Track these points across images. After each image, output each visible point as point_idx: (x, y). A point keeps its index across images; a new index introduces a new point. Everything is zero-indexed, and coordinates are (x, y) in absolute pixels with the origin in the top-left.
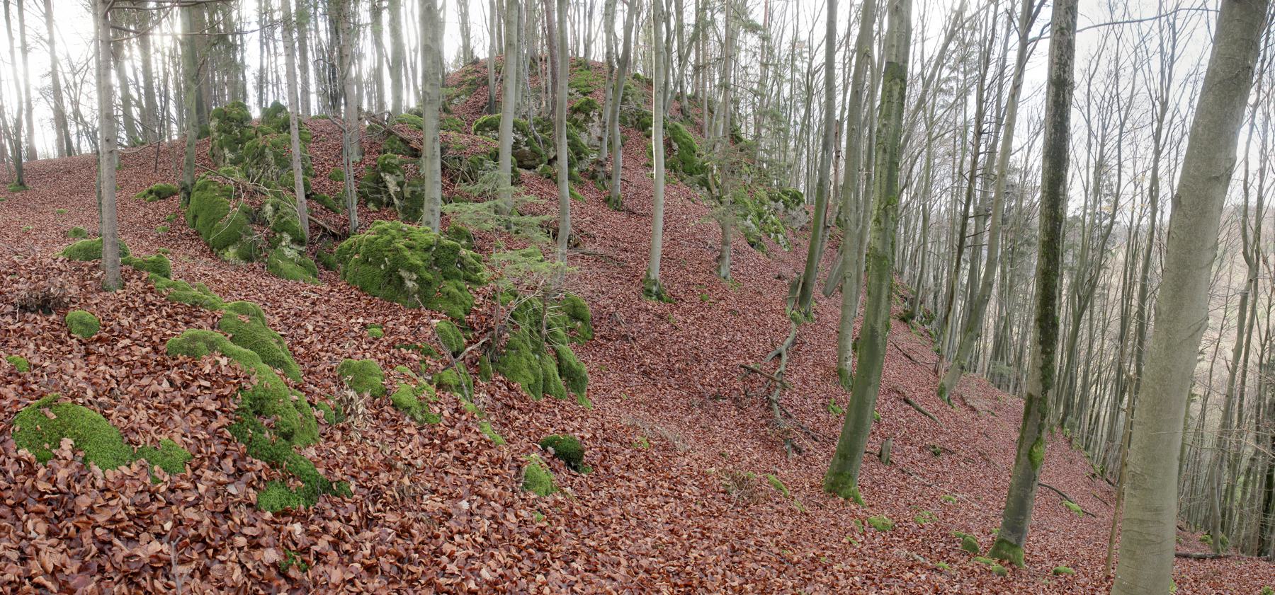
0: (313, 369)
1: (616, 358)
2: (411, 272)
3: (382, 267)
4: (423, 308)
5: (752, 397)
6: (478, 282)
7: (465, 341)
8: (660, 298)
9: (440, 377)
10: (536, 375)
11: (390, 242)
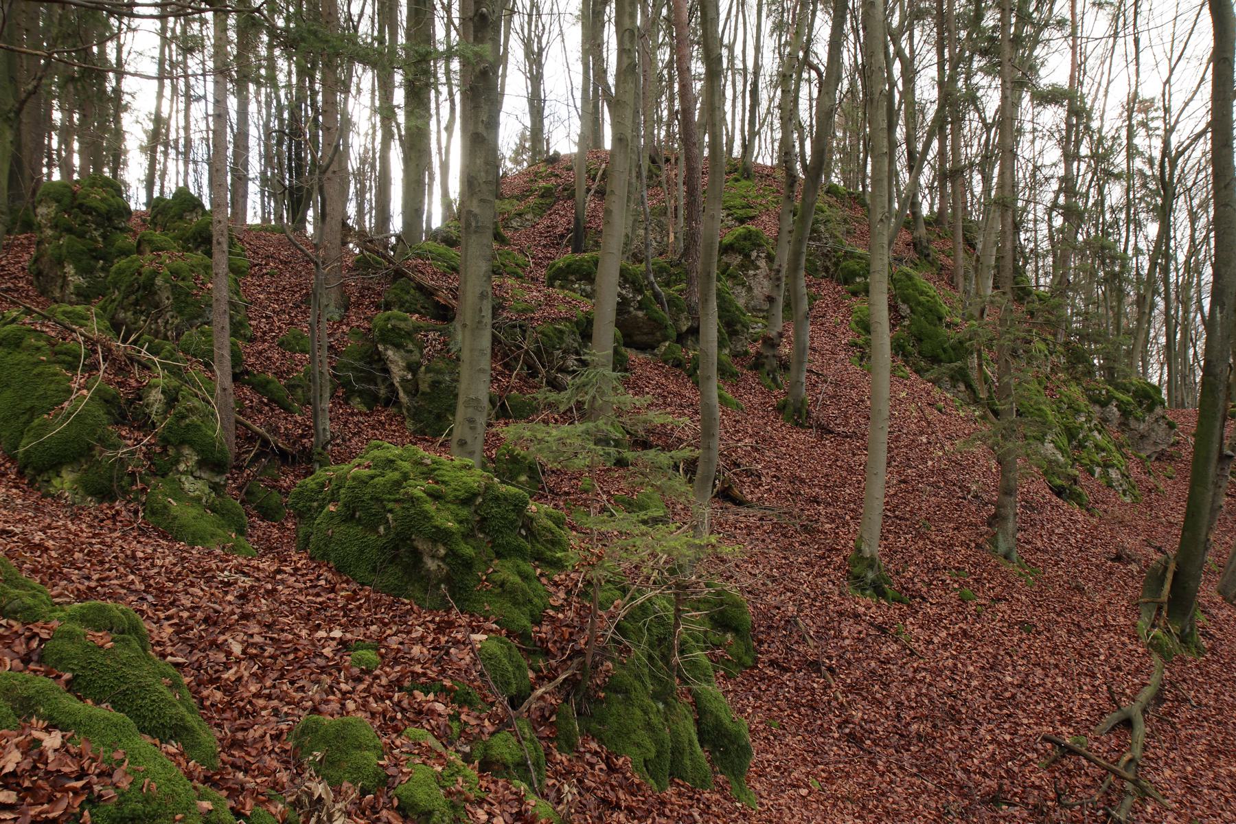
0: (240, 735)
1: (796, 706)
2: (435, 542)
3: (382, 529)
4: (456, 610)
5: (1071, 807)
6: (558, 565)
7: (531, 674)
8: (879, 592)
9: (487, 747)
10: (659, 743)
11: (398, 484)
